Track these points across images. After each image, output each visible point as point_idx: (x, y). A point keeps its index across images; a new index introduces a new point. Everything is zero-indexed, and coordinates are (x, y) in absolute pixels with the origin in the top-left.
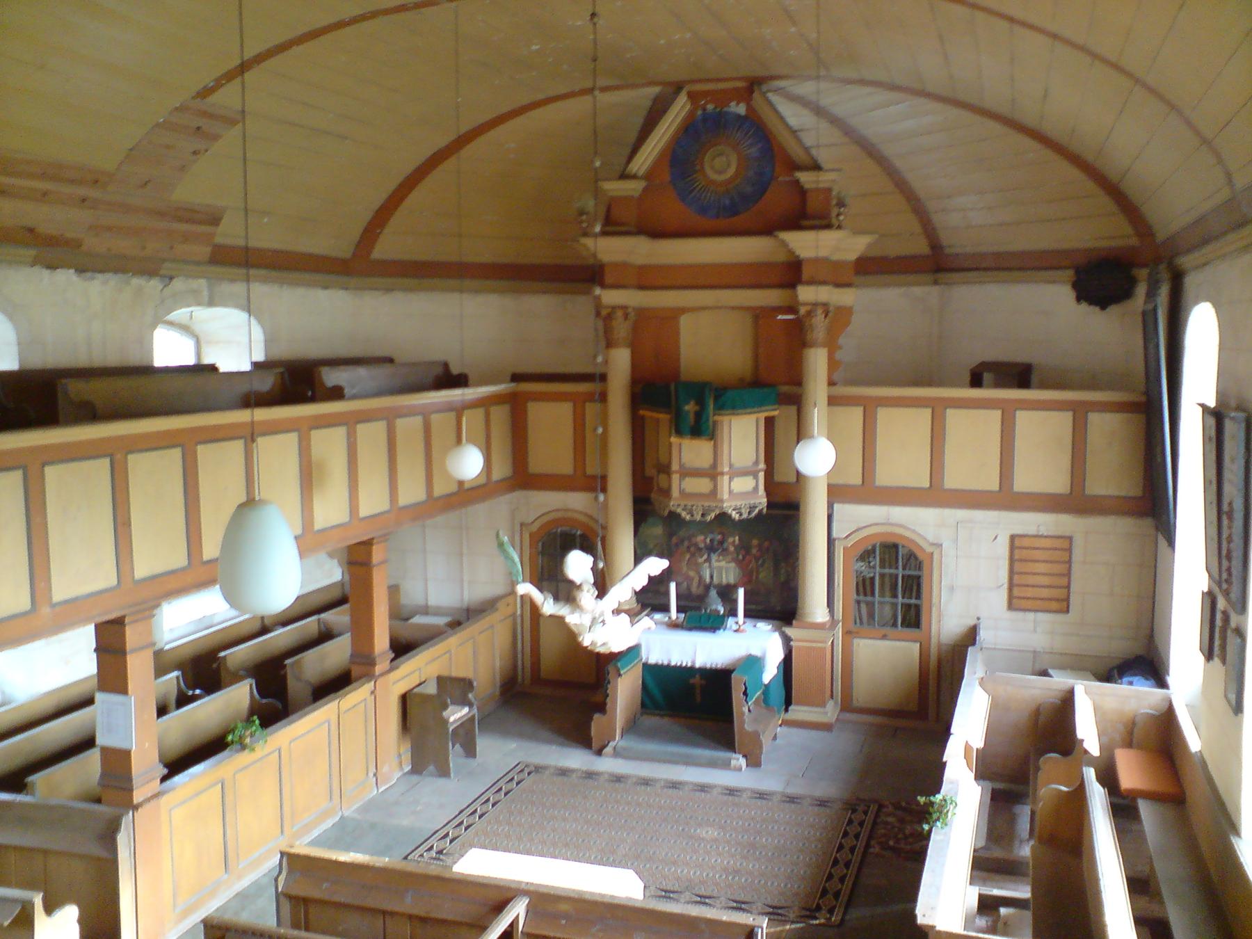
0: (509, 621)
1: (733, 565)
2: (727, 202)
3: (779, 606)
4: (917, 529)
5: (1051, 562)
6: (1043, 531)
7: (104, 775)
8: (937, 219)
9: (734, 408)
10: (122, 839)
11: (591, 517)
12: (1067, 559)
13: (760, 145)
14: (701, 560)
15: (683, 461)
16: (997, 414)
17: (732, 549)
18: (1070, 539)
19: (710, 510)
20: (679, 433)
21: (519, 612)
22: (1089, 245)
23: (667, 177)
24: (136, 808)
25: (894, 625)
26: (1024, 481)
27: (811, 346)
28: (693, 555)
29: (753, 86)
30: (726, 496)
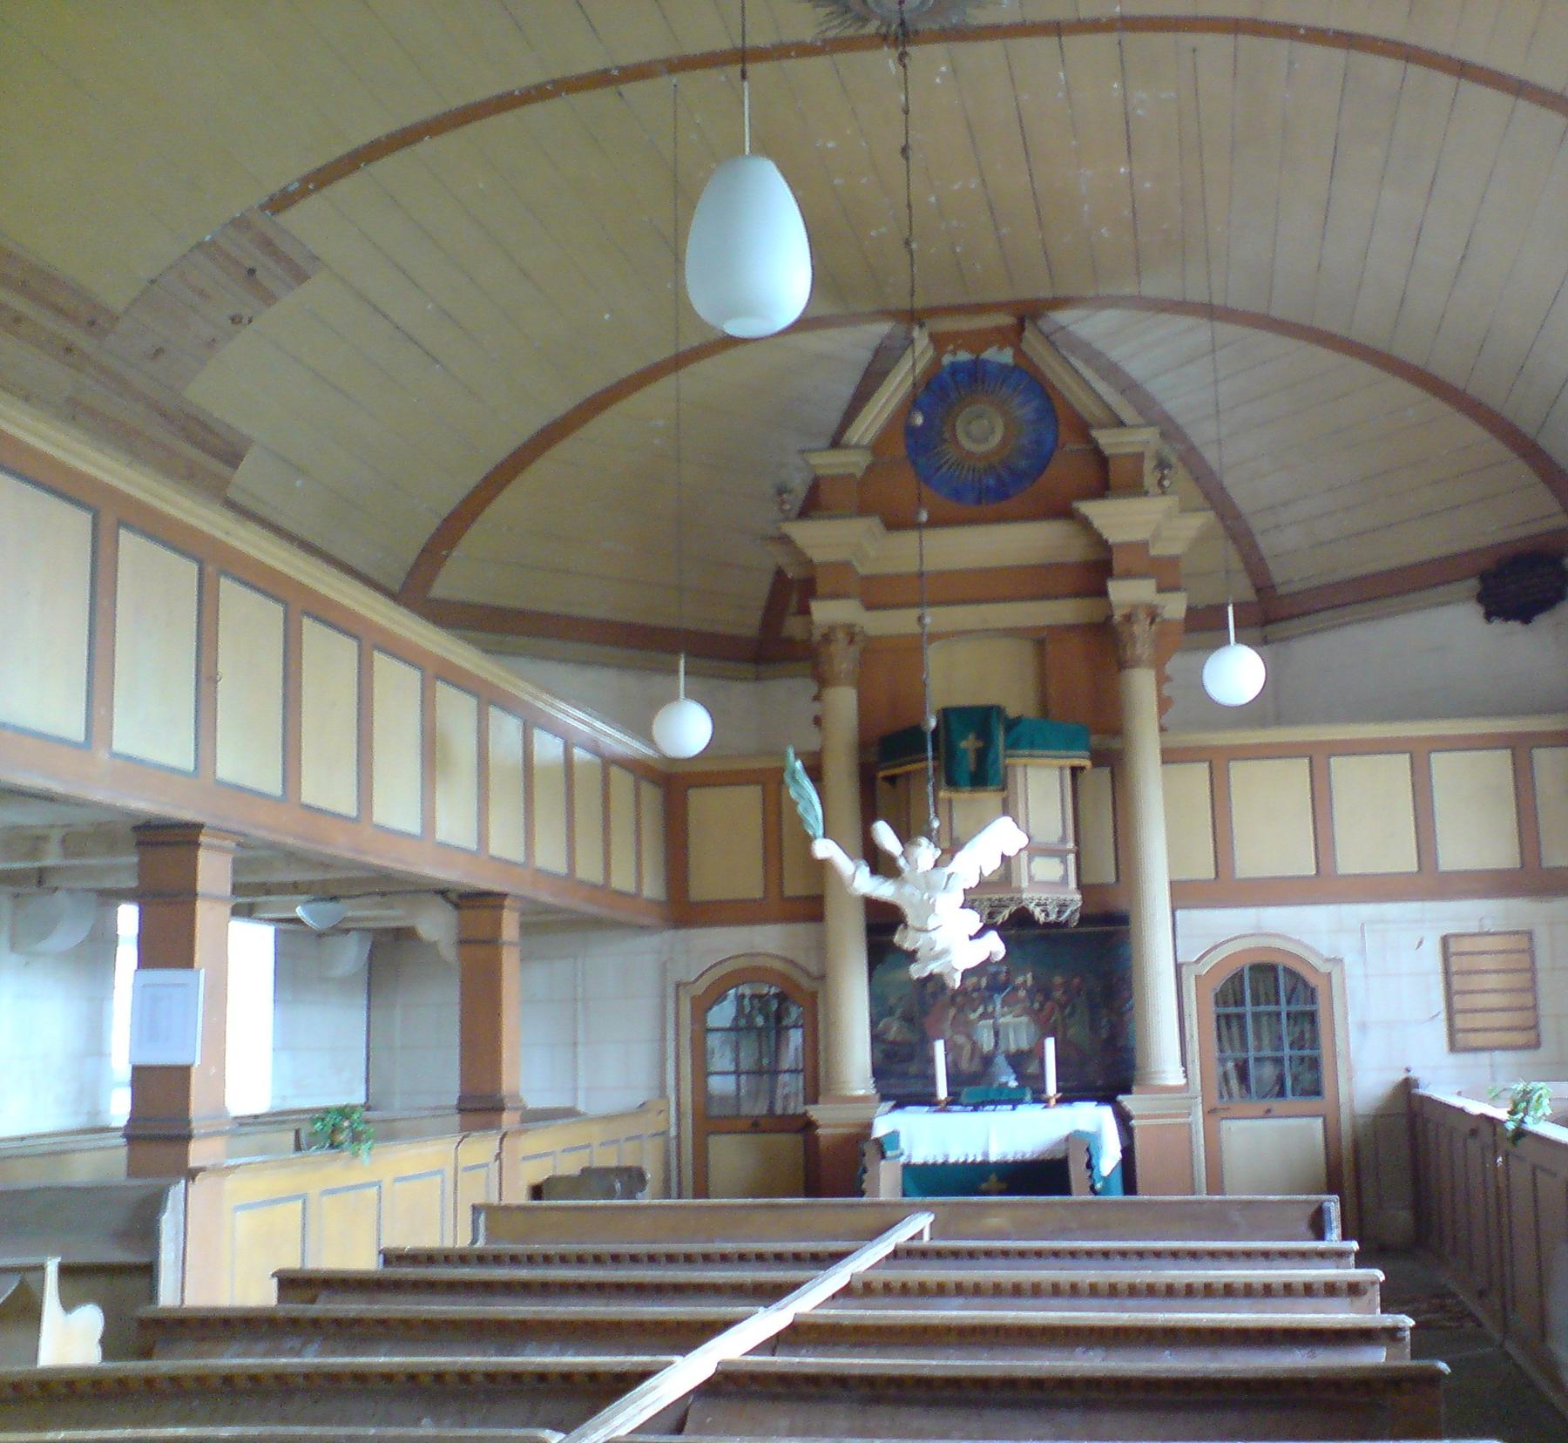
0: (659, 1140)
1: (1024, 1019)
2: (992, 482)
3: (1106, 1071)
4: (1307, 940)
5: (1504, 971)
6: (1489, 926)
7: (133, 1119)
8: (1266, 544)
9: (1032, 746)
10: (168, 1224)
11: (792, 962)
12: (1526, 965)
13: (1035, 404)
14: (973, 1016)
15: (955, 834)
16: (1405, 759)
17: (1022, 993)
18: (1530, 934)
19: (1001, 905)
20: (952, 783)
21: (673, 1132)
22: (1501, 537)
23: (901, 451)
24: (192, 1175)
25: (1281, 1093)
26: (1455, 854)
27: (1132, 667)
28: (961, 1009)
29: (1027, 314)
30: (1025, 884)
